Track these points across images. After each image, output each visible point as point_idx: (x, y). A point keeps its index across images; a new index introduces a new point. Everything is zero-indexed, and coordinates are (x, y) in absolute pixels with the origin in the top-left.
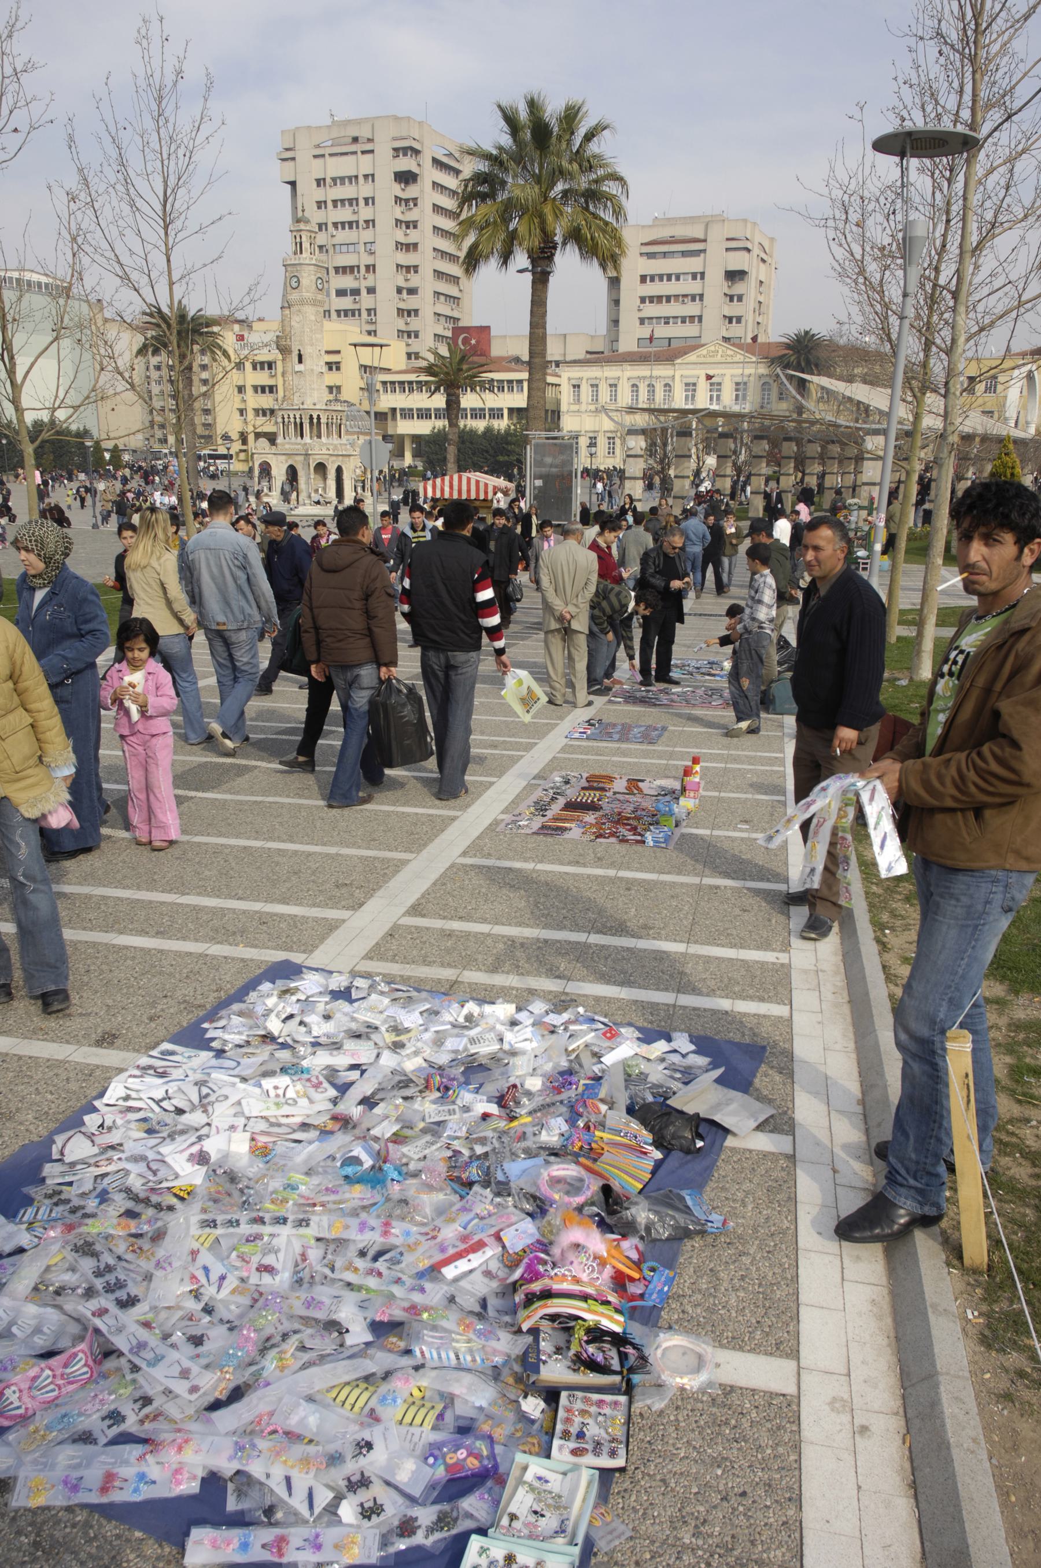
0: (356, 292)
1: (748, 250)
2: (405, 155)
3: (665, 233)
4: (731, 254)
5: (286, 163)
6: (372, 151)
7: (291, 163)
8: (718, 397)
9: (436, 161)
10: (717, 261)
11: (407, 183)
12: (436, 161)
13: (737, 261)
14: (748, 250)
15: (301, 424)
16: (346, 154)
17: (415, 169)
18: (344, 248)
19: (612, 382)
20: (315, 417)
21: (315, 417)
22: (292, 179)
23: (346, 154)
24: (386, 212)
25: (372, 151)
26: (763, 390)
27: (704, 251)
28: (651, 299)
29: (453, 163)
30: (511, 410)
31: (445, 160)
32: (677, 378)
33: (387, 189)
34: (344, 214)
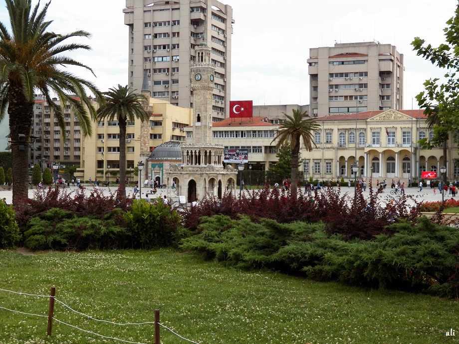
0: (166, 82)
1: (391, 60)
2: (197, 10)
3: (344, 51)
4: (381, 62)
5: (128, 15)
6: (179, 9)
7: (131, 15)
8: (393, 139)
9: (213, 14)
10: (373, 68)
11: (198, 25)
12: (213, 14)
13: (386, 66)
14: (391, 60)
15: (199, 156)
16: (164, 10)
17: (202, 18)
18: (347, 63)
19: (328, 131)
20: (208, 152)
21: (208, 152)
22: (131, 23)
23: (164, 10)
24: (185, 40)
26: (341, 137)
27: (329, 57)
28: (337, 75)
29: (222, 15)
30: (266, 147)
31: (218, 13)
32: (369, 130)
33: (185, 28)
34: (158, 30)
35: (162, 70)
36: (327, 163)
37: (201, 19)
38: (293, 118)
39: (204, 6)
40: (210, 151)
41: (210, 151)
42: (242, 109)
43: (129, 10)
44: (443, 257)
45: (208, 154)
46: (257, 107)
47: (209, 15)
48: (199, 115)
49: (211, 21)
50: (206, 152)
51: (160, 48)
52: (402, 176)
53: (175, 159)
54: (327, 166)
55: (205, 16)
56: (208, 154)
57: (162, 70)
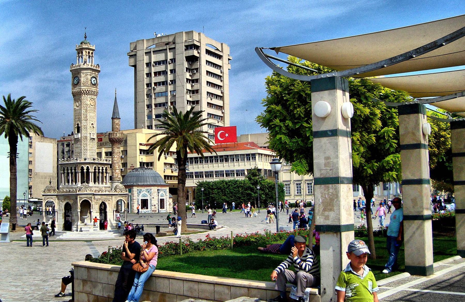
25: (175, 48)
35: (162, 105)
36: (308, 184)
37: (194, 55)
38: (5, 107)
39: (198, 44)
40: (88, 167)
41: (88, 167)
42: (227, 135)
43: (133, 54)
44: (289, 287)
45: (85, 170)
46: (420, 154)
47: (203, 52)
48: (78, 124)
49: (205, 57)
50: (82, 169)
51: (160, 85)
52: (383, 193)
53: (142, 184)
54: (309, 187)
55: (198, 53)
56: (85, 170)
57: (162, 105)
